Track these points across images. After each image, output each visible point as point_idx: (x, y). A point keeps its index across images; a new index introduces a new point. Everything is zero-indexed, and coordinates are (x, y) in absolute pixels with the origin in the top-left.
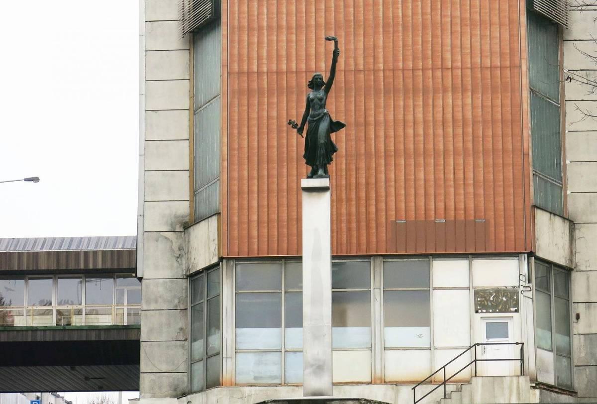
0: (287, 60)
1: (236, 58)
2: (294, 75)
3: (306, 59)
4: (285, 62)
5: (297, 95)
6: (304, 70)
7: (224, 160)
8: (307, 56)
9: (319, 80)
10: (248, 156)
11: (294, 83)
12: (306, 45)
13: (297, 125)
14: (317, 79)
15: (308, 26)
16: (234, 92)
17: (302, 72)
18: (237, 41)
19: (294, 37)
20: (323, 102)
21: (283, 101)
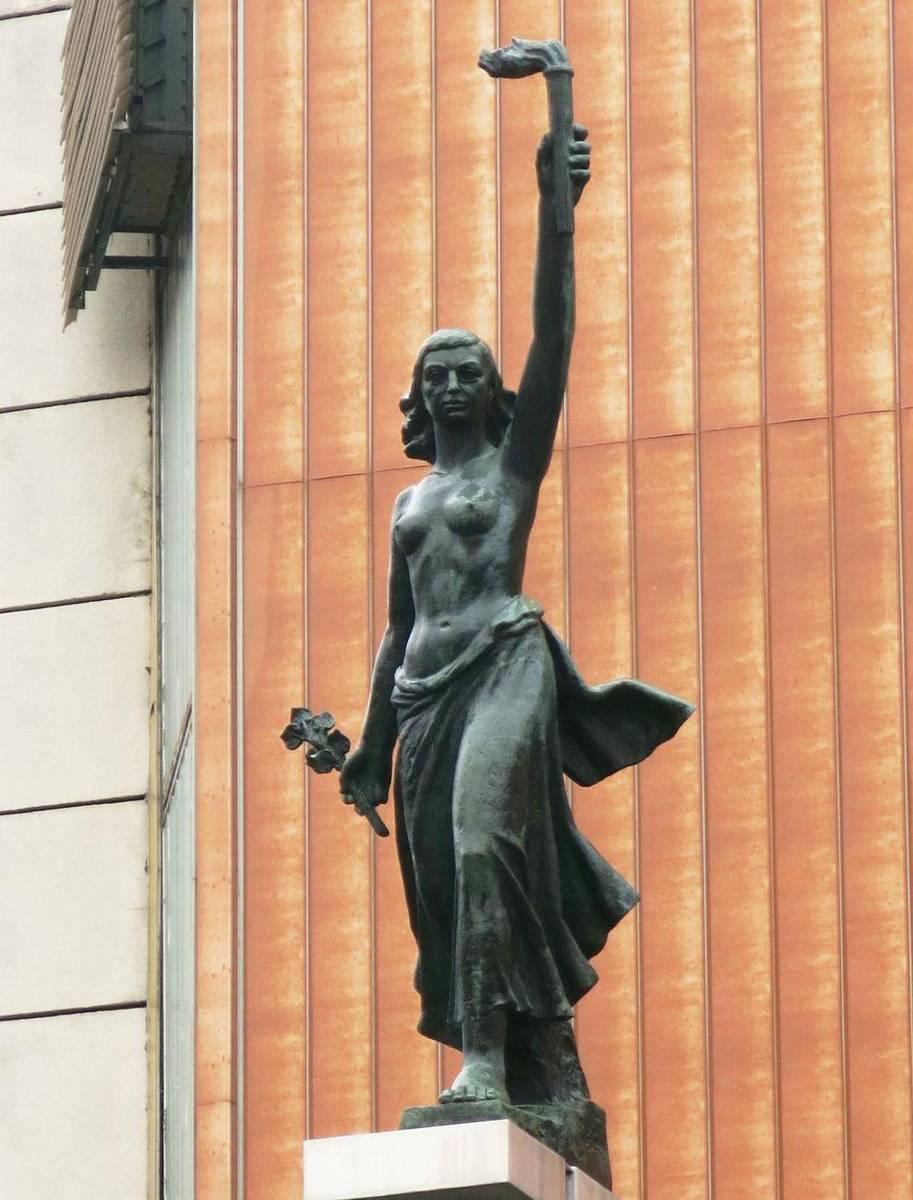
0: (634, 359)
1: (292, 381)
2: (685, 456)
3: (765, 342)
4: (623, 370)
5: (705, 598)
6: (751, 416)
7: (211, 1103)
8: (773, 308)
9: (453, 382)
10: (376, 1057)
11: (683, 515)
12: (763, 238)
13: (339, 740)
14: (439, 375)
15: (772, 105)
16: (275, 616)
17: (735, 430)
18: (296, 264)
19: (678, 191)
20: (494, 546)
21: (612, 650)
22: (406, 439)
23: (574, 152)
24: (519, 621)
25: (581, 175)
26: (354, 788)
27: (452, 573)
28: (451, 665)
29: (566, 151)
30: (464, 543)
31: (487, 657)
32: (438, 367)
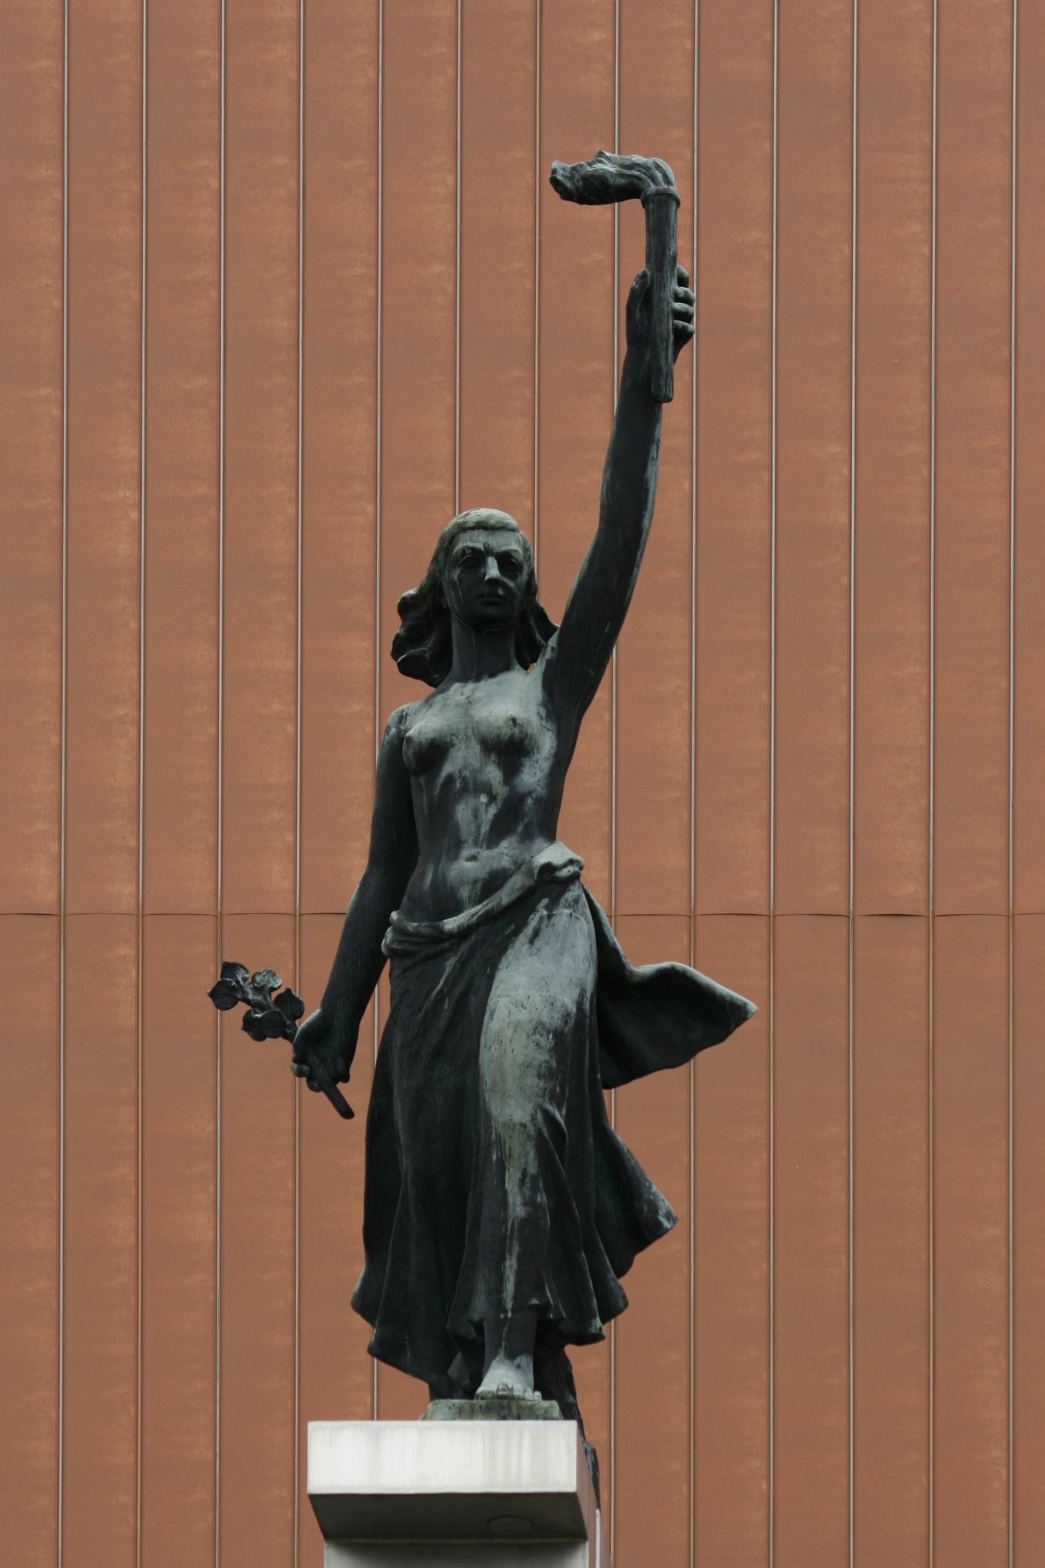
9: (493, 570)
13: (290, 1003)
14: (476, 558)
22: (395, 654)
23: (678, 299)
24: (565, 866)
25: (685, 329)
26: (314, 1059)
27: (484, 799)
28: (479, 907)
29: (668, 294)
30: (500, 764)
31: (524, 905)
32: (474, 550)
